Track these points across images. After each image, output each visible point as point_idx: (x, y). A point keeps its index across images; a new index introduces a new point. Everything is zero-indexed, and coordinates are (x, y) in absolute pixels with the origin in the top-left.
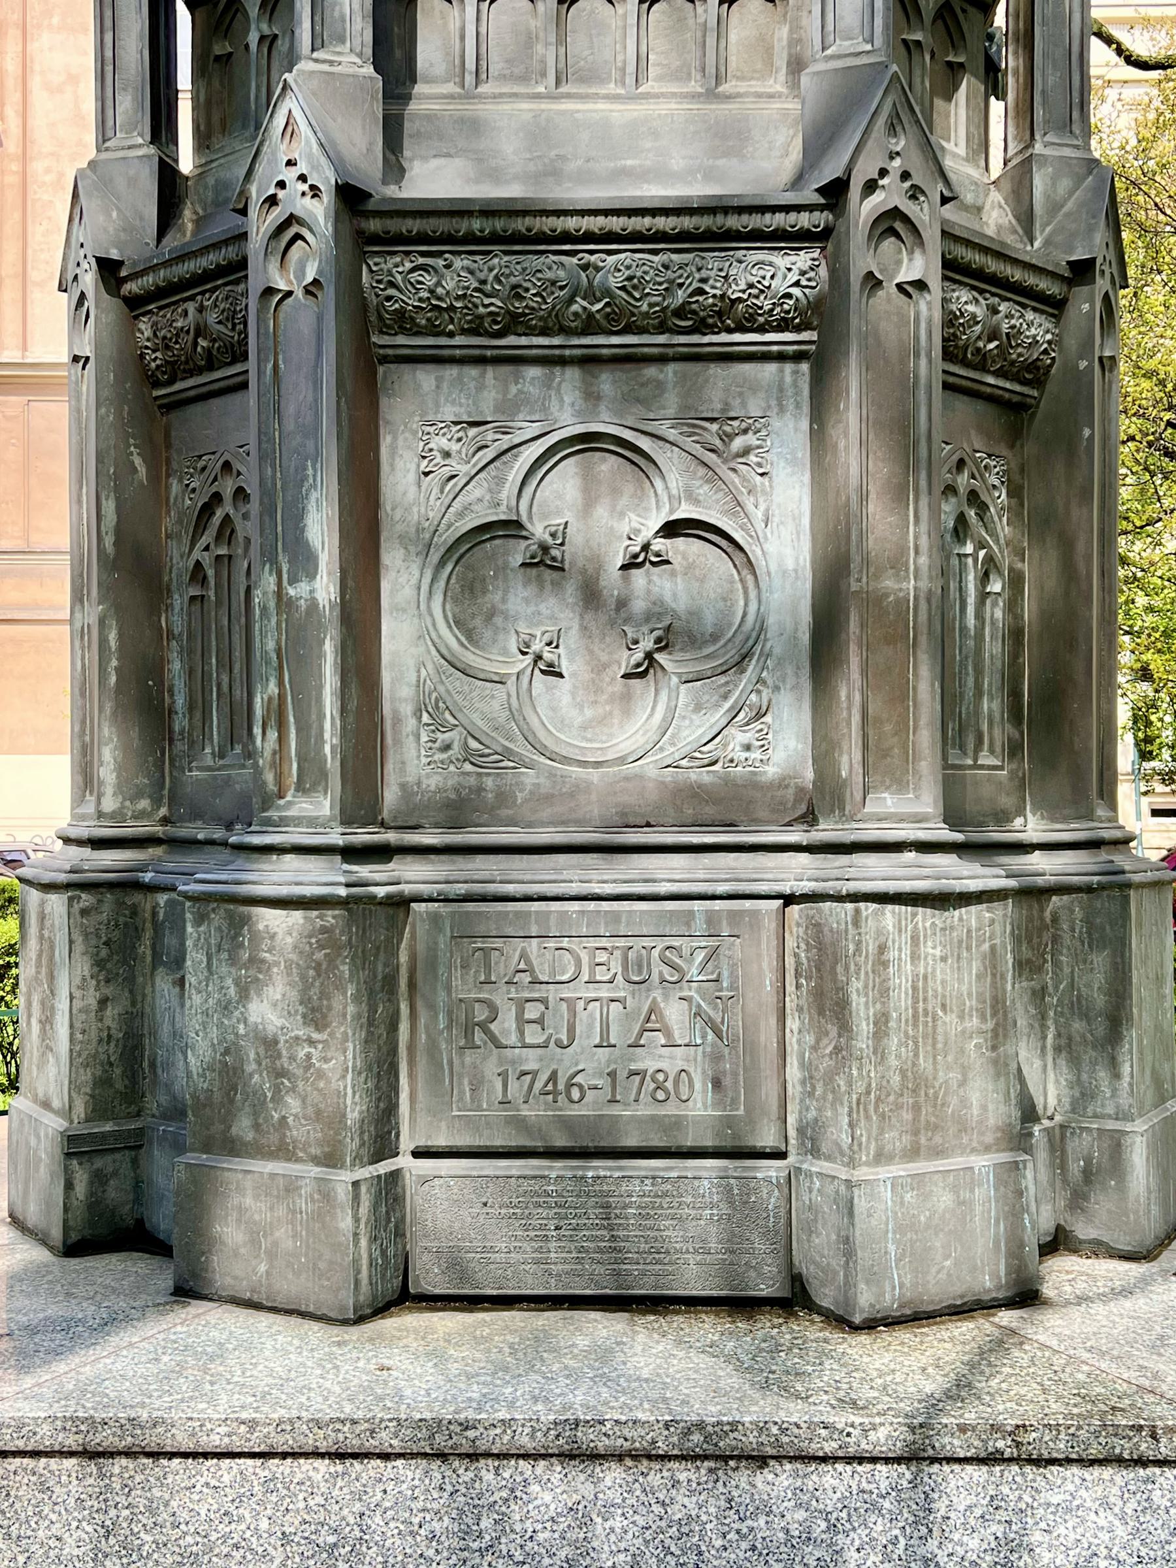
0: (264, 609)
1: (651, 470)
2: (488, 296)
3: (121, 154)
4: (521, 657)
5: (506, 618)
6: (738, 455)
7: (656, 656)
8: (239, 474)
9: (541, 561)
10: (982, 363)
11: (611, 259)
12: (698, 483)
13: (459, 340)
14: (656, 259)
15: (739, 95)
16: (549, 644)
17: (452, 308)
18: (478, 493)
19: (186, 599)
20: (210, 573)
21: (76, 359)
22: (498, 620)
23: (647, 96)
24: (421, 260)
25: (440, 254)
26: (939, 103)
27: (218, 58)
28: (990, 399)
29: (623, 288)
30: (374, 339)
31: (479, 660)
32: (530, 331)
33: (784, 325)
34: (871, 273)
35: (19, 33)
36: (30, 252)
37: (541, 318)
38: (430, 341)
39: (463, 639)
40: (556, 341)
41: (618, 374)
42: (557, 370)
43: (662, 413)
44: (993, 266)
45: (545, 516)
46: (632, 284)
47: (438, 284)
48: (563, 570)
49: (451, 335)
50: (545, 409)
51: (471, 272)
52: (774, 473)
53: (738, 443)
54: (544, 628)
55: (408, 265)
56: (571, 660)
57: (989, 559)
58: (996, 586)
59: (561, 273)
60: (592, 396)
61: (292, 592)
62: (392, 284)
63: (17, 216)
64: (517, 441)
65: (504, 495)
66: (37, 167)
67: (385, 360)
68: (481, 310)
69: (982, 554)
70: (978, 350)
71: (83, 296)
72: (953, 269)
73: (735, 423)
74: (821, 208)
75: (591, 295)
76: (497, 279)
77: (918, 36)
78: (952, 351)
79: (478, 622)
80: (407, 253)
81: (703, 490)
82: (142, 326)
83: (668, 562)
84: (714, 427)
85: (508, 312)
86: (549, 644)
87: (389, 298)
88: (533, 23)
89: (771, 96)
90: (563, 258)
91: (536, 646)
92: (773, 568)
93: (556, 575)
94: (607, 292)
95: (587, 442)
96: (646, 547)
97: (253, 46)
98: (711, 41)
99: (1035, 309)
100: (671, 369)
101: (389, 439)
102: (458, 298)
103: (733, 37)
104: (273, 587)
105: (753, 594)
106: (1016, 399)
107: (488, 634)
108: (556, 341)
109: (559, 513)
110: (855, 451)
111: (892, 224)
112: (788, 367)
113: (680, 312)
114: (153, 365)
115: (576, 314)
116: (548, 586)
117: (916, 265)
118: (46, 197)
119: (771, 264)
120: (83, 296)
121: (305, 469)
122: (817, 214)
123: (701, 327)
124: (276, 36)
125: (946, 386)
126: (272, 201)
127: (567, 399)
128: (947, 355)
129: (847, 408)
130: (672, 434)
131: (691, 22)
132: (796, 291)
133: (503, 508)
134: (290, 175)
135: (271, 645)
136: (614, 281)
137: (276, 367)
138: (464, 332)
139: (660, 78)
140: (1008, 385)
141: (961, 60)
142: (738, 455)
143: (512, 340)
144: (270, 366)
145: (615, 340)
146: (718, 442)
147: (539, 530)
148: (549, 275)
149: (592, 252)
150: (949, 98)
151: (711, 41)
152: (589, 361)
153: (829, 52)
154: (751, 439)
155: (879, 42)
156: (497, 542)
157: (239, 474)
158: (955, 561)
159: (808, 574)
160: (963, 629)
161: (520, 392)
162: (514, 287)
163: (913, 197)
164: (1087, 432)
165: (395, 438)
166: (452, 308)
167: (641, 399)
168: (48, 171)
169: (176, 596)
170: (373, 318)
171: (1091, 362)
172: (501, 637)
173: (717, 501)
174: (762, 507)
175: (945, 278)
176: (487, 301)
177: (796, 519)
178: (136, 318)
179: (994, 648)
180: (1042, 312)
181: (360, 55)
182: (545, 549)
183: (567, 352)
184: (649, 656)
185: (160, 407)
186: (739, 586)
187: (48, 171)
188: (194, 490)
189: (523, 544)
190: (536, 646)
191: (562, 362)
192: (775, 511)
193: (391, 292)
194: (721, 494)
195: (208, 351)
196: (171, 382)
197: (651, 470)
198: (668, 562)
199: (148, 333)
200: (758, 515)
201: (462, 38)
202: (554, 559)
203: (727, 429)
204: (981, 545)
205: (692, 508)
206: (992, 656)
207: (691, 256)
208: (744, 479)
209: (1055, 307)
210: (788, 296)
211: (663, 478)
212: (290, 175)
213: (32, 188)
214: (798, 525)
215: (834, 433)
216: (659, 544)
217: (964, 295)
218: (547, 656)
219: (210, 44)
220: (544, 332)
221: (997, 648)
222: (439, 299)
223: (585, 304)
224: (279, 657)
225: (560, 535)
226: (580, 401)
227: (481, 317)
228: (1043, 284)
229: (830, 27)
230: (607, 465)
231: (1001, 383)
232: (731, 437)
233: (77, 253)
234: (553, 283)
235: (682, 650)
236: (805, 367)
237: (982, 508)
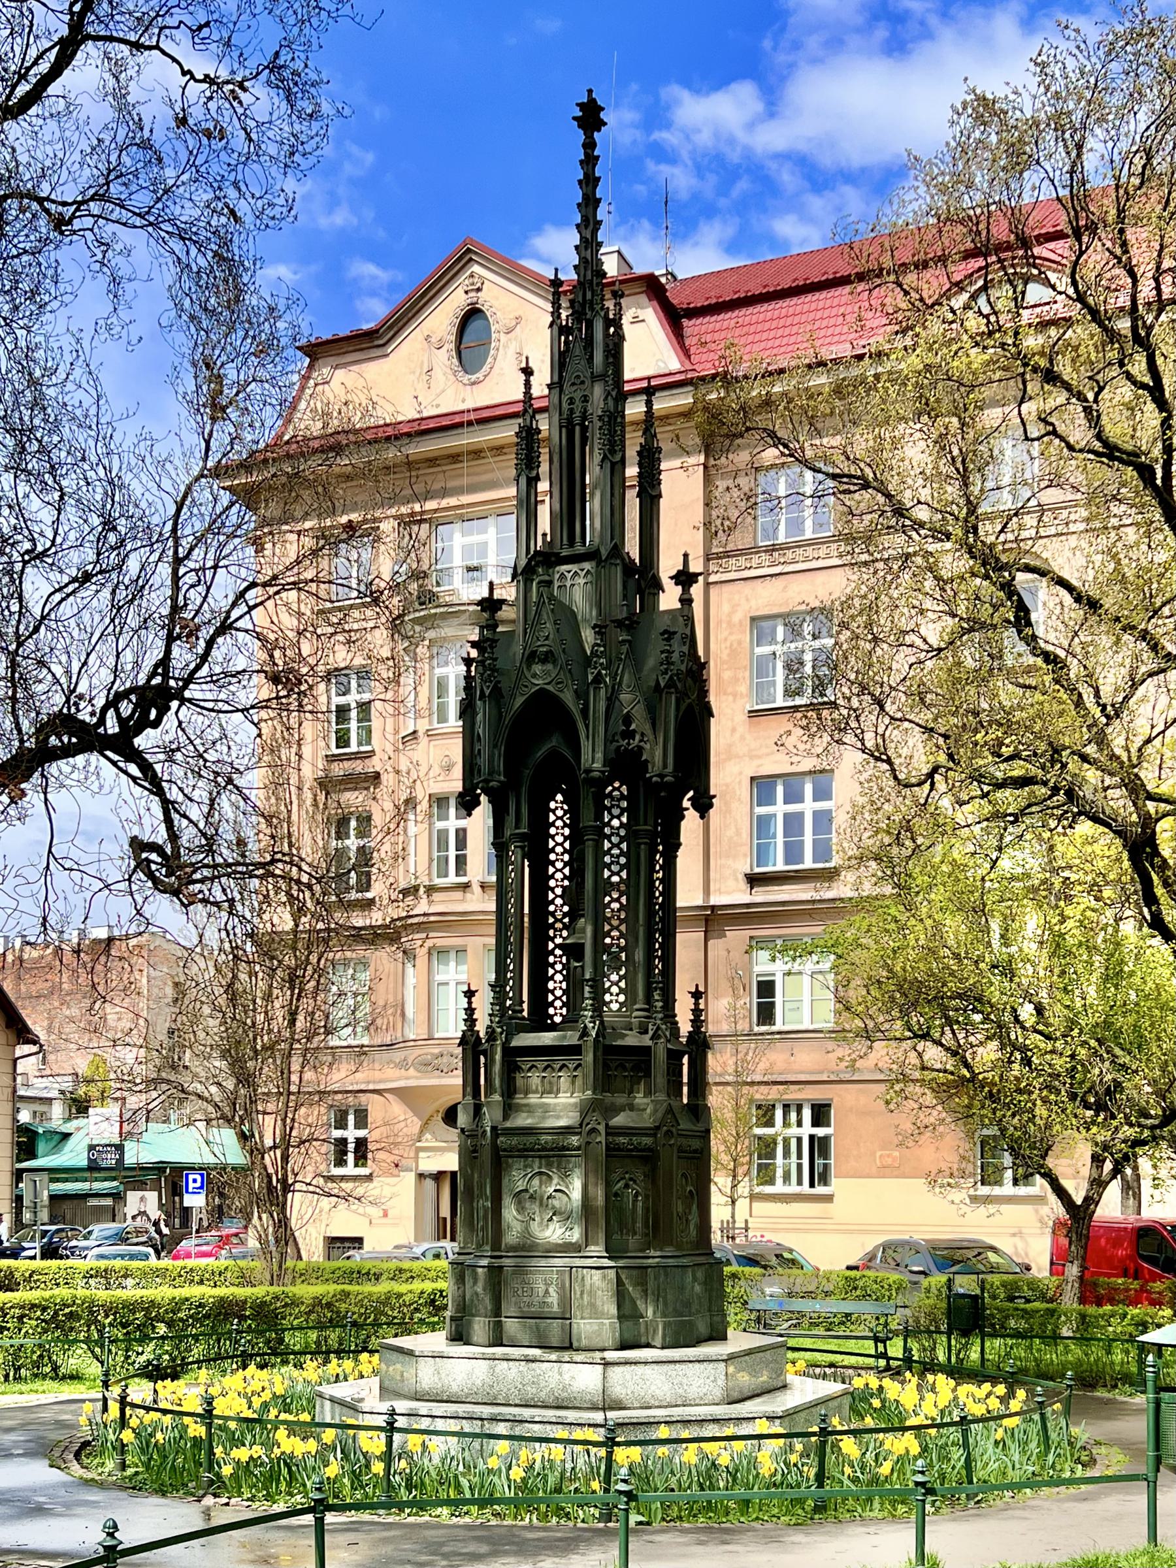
95: (540, 1173)
152: (540, 1157)
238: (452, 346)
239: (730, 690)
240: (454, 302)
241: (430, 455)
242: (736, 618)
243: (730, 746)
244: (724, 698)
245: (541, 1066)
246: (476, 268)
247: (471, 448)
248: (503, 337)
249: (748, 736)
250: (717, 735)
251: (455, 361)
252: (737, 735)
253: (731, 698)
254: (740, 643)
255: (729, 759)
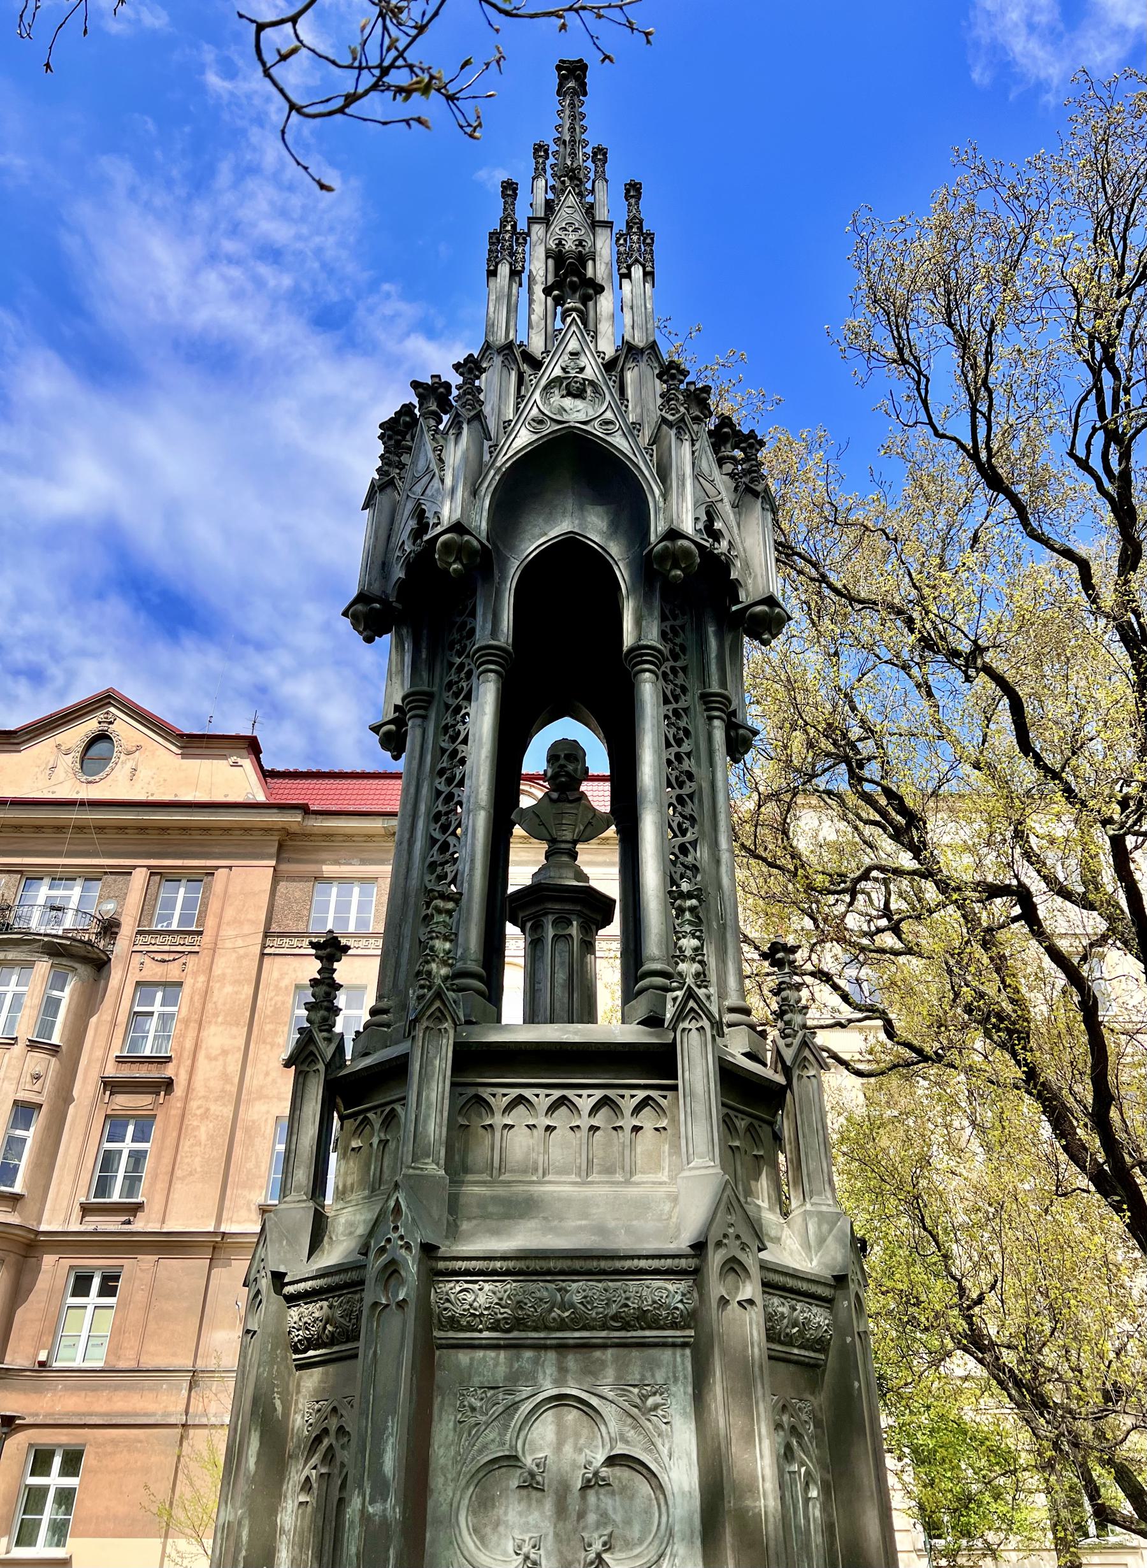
0: (352, 1522)
1: (598, 1420)
2: (503, 1307)
3: (292, 1205)
4: (515, 1557)
5: (507, 1527)
6: (651, 1410)
7: (604, 1556)
8: (342, 1416)
9: (530, 1485)
10: (790, 1341)
11: (575, 1285)
12: (627, 1429)
13: (486, 1334)
14: (600, 1285)
15: (643, 1183)
16: (534, 1547)
17: (482, 1315)
18: (492, 1436)
19: (296, 1504)
20: (315, 1485)
21: (248, 1332)
22: (501, 1529)
23: (592, 1183)
24: (466, 1286)
25: (476, 1282)
26: (753, 1183)
27: (353, 1149)
28: (796, 1363)
29: (581, 1303)
30: (436, 1334)
31: (488, 1560)
32: (526, 1328)
33: (674, 1326)
34: (722, 1297)
35: (197, 1026)
36: (179, 1157)
37: (533, 1321)
38: (468, 1335)
39: (478, 1543)
40: (542, 1335)
41: (578, 1356)
42: (543, 1353)
43: (605, 1381)
44: (791, 1283)
45: (533, 1452)
46: (587, 1301)
47: (475, 1300)
48: (543, 1490)
49: (481, 1331)
50: (535, 1378)
51: (494, 1293)
52: (673, 1422)
53: (650, 1401)
54: (531, 1535)
55: (458, 1289)
56: (548, 1559)
57: (808, 1473)
58: (814, 1493)
59: (545, 1294)
60: (562, 1370)
61: (371, 1510)
62: (448, 1300)
63: (175, 1134)
64: (517, 1399)
65: (508, 1438)
66: (193, 1104)
67: (440, 1347)
68: (499, 1316)
69: (803, 1470)
70: (787, 1334)
71: (258, 1292)
72: (766, 1285)
73: (648, 1388)
74: (693, 1256)
75: (563, 1307)
76: (509, 1297)
77: (737, 1143)
78: (772, 1335)
79: (488, 1530)
80: (458, 1281)
81: (631, 1434)
82: (292, 1313)
83: (609, 1485)
84: (636, 1391)
85: (515, 1318)
86: (534, 1547)
87: (445, 1309)
88: (531, 1141)
89: (661, 1183)
90: (548, 1284)
91: (525, 1550)
92: (676, 1490)
93: (539, 1494)
94: (572, 1306)
95: (560, 1400)
96: (596, 1474)
97: (375, 1146)
98: (627, 1152)
99: (817, 1305)
100: (610, 1352)
101: (439, 1399)
102: (486, 1309)
103: (639, 1150)
104: (359, 1506)
105: (664, 1509)
106: (812, 1361)
107: (494, 1538)
108: (542, 1335)
109: (541, 1449)
110: (721, 1411)
111: (733, 1267)
112: (679, 1352)
113: (615, 1318)
114: (296, 1339)
115: (554, 1319)
116: (534, 1503)
117: (749, 1290)
118: (195, 1123)
119: (666, 1289)
120: (258, 1292)
121: (387, 1422)
122: (690, 1260)
123: (626, 1327)
124: (388, 1141)
125: (770, 1358)
126: (383, 1250)
127: (548, 1372)
128: (770, 1338)
129: (714, 1382)
130: (611, 1395)
131: (616, 1141)
132: (680, 1305)
133: (507, 1446)
134: (393, 1236)
135: (353, 1550)
136: (577, 1299)
137: (375, 1352)
138: (488, 1329)
139: (599, 1173)
140: (806, 1354)
141: (761, 1153)
142: (651, 1410)
143: (515, 1334)
144: (371, 1352)
145: (577, 1334)
146: (638, 1401)
147: (528, 1461)
148: (538, 1294)
149: (563, 1281)
150: (757, 1180)
151: (627, 1152)
152: (562, 1347)
153: (691, 1165)
154: (657, 1399)
155: (718, 1161)
156: (503, 1470)
157: (342, 1416)
158: (787, 1476)
159: (697, 1494)
160: (797, 1527)
161: (520, 1366)
162: (518, 1302)
163: (743, 1249)
164: (856, 1384)
165: (443, 1399)
166: (482, 1315)
167: (591, 1371)
168: (199, 1107)
169: (290, 1502)
170: (435, 1321)
171: (853, 1338)
172: (503, 1541)
173: (639, 1442)
174: (667, 1446)
175: (764, 1292)
176: (502, 1310)
177: (689, 1455)
178: (289, 1307)
179: (817, 1539)
180: (821, 1306)
181: (437, 1164)
182: (532, 1475)
183: (549, 1342)
184: (599, 1556)
185: (296, 1366)
186: (655, 1502)
187: (199, 1107)
188: (311, 1425)
189: (519, 1471)
190: (525, 1550)
191: (546, 1347)
192: (675, 1449)
193: (447, 1305)
194: (641, 1437)
195: (332, 1333)
196: (305, 1351)
197: (598, 1420)
198: (609, 1485)
199: (296, 1319)
200: (665, 1451)
201: (493, 1150)
202: (538, 1483)
203: (644, 1392)
204: (802, 1464)
205: (624, 1446)
206: (817, 1546)
207: (619, 1284)
208: (656, 1427)
209: (828, 1302)
210: (677, 1308)
211: (606, 1424)
212: (393, 1236)
213: (188, 1116)
214: (690, 1459)
215: (709, 1398)
216: (605, 1472)
217: (776, 1301)
218: (532, 1556)
219: (350, 1140)
220: (536, 1329)
221: (819, 1540)
222: (475, 1309)
223: (559, 1312)
224: (358, 1558)
225: (541, 1464)
226: (555, 1373)
227: (498, 1321)
228: (820, 1290)
229: (691, 1151)
230: (572, 1416)
231: (803, 1352)
232: (646, 1397)
233: (259, 1265)
234: (541, 1300)
235: (620, 1551)
236: (688, 1352)
237: (799, 1436)
238: (78, 755)
239: (269, 1040)
240: (90, 726)
241: (38, 823)
242: (283, 984)
243: (262, 1087)
244: (262, 1046)
245: (543, 1099)
246: (112, 709)
247: (79, 823)
248: (123, 757)
249: (279, 1081)
250: (252, 1077)
251: (78, 765)
252: (269, 1079)
253: (268, 1047)
254: (283, 1003)
255: (259, 1098)
